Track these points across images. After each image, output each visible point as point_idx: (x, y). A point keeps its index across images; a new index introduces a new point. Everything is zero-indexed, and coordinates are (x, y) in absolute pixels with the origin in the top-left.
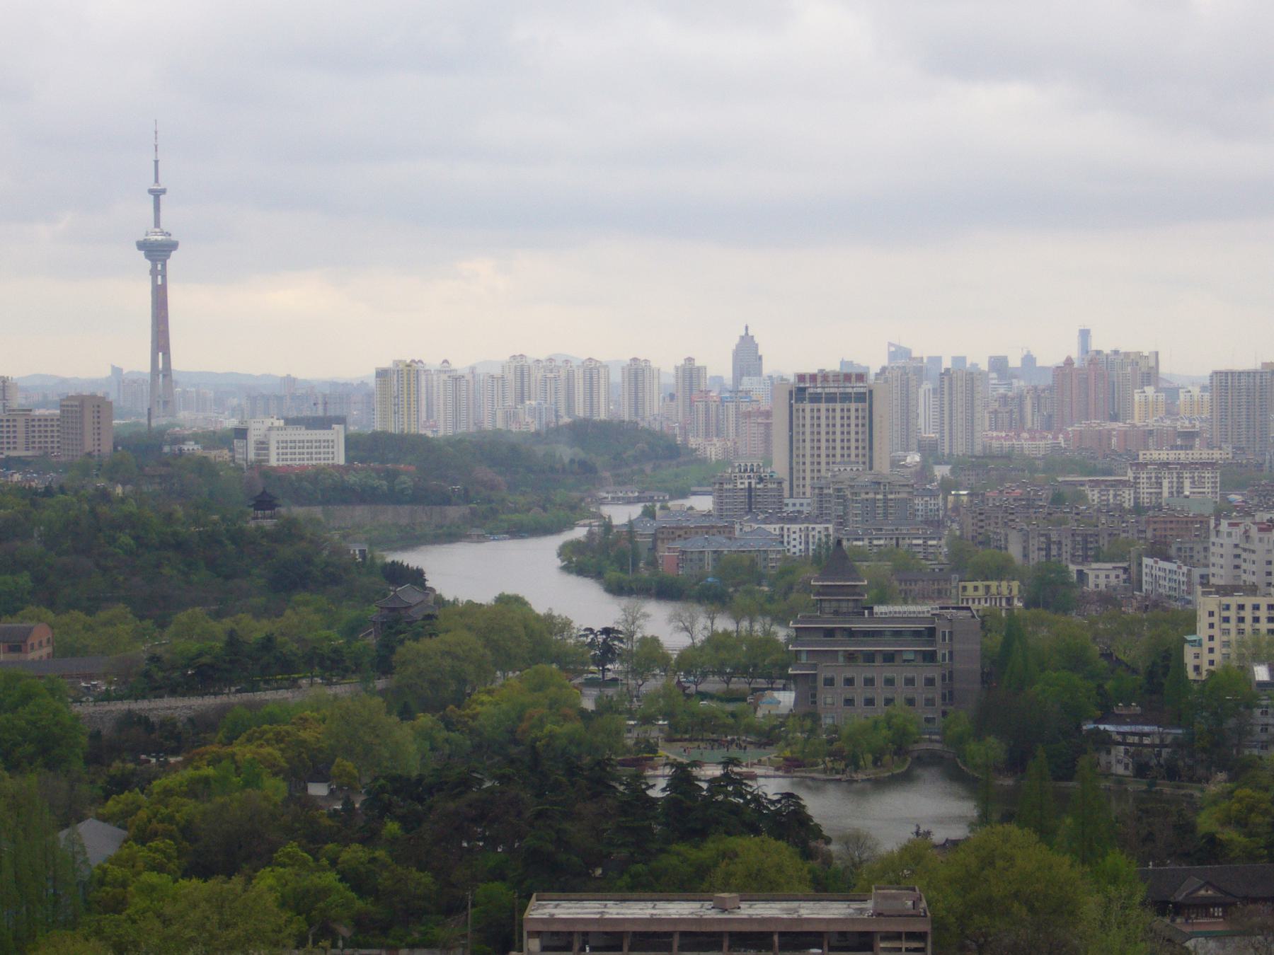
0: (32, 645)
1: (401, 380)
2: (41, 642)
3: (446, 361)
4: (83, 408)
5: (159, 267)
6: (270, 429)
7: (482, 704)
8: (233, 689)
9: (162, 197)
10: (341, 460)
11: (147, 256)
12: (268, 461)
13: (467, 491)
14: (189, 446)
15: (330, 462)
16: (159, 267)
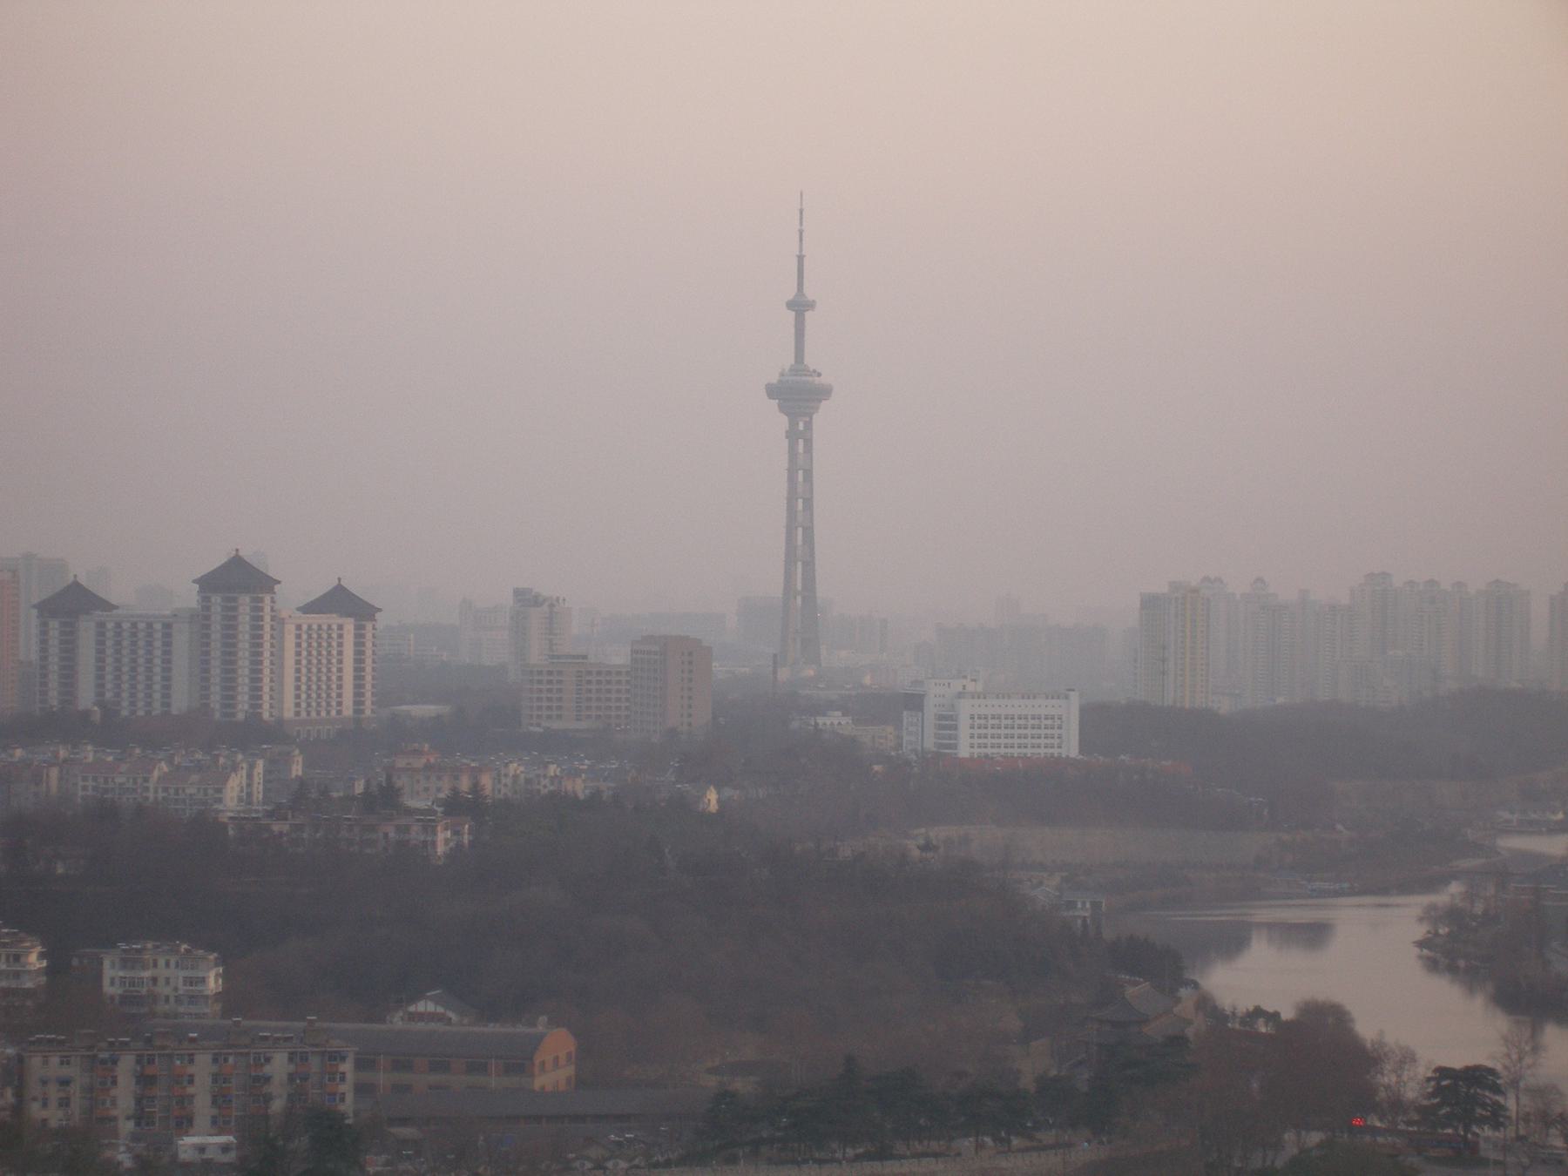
0: (543, 1063)
1: (1173, 615)
2: (556, 1059)
3: (1260, 580)
4: (670, 656)
5: (801, 426)
6: (960, 695)
7: (1374, 1131)
8: (850, 1152)
9: (808, 314)
10: (1071, 749)
11: (782, 409)
12: (955, 747)
13: (605, 1169)
14: (834, 721)
15: (1056, 751)
16: (801, 426)
